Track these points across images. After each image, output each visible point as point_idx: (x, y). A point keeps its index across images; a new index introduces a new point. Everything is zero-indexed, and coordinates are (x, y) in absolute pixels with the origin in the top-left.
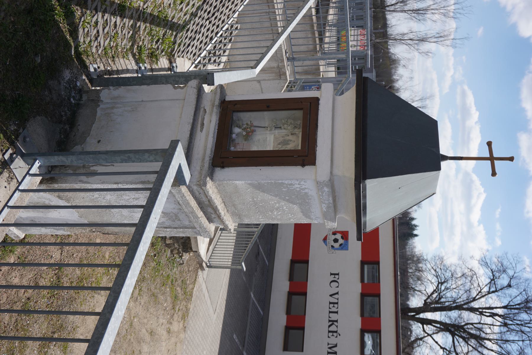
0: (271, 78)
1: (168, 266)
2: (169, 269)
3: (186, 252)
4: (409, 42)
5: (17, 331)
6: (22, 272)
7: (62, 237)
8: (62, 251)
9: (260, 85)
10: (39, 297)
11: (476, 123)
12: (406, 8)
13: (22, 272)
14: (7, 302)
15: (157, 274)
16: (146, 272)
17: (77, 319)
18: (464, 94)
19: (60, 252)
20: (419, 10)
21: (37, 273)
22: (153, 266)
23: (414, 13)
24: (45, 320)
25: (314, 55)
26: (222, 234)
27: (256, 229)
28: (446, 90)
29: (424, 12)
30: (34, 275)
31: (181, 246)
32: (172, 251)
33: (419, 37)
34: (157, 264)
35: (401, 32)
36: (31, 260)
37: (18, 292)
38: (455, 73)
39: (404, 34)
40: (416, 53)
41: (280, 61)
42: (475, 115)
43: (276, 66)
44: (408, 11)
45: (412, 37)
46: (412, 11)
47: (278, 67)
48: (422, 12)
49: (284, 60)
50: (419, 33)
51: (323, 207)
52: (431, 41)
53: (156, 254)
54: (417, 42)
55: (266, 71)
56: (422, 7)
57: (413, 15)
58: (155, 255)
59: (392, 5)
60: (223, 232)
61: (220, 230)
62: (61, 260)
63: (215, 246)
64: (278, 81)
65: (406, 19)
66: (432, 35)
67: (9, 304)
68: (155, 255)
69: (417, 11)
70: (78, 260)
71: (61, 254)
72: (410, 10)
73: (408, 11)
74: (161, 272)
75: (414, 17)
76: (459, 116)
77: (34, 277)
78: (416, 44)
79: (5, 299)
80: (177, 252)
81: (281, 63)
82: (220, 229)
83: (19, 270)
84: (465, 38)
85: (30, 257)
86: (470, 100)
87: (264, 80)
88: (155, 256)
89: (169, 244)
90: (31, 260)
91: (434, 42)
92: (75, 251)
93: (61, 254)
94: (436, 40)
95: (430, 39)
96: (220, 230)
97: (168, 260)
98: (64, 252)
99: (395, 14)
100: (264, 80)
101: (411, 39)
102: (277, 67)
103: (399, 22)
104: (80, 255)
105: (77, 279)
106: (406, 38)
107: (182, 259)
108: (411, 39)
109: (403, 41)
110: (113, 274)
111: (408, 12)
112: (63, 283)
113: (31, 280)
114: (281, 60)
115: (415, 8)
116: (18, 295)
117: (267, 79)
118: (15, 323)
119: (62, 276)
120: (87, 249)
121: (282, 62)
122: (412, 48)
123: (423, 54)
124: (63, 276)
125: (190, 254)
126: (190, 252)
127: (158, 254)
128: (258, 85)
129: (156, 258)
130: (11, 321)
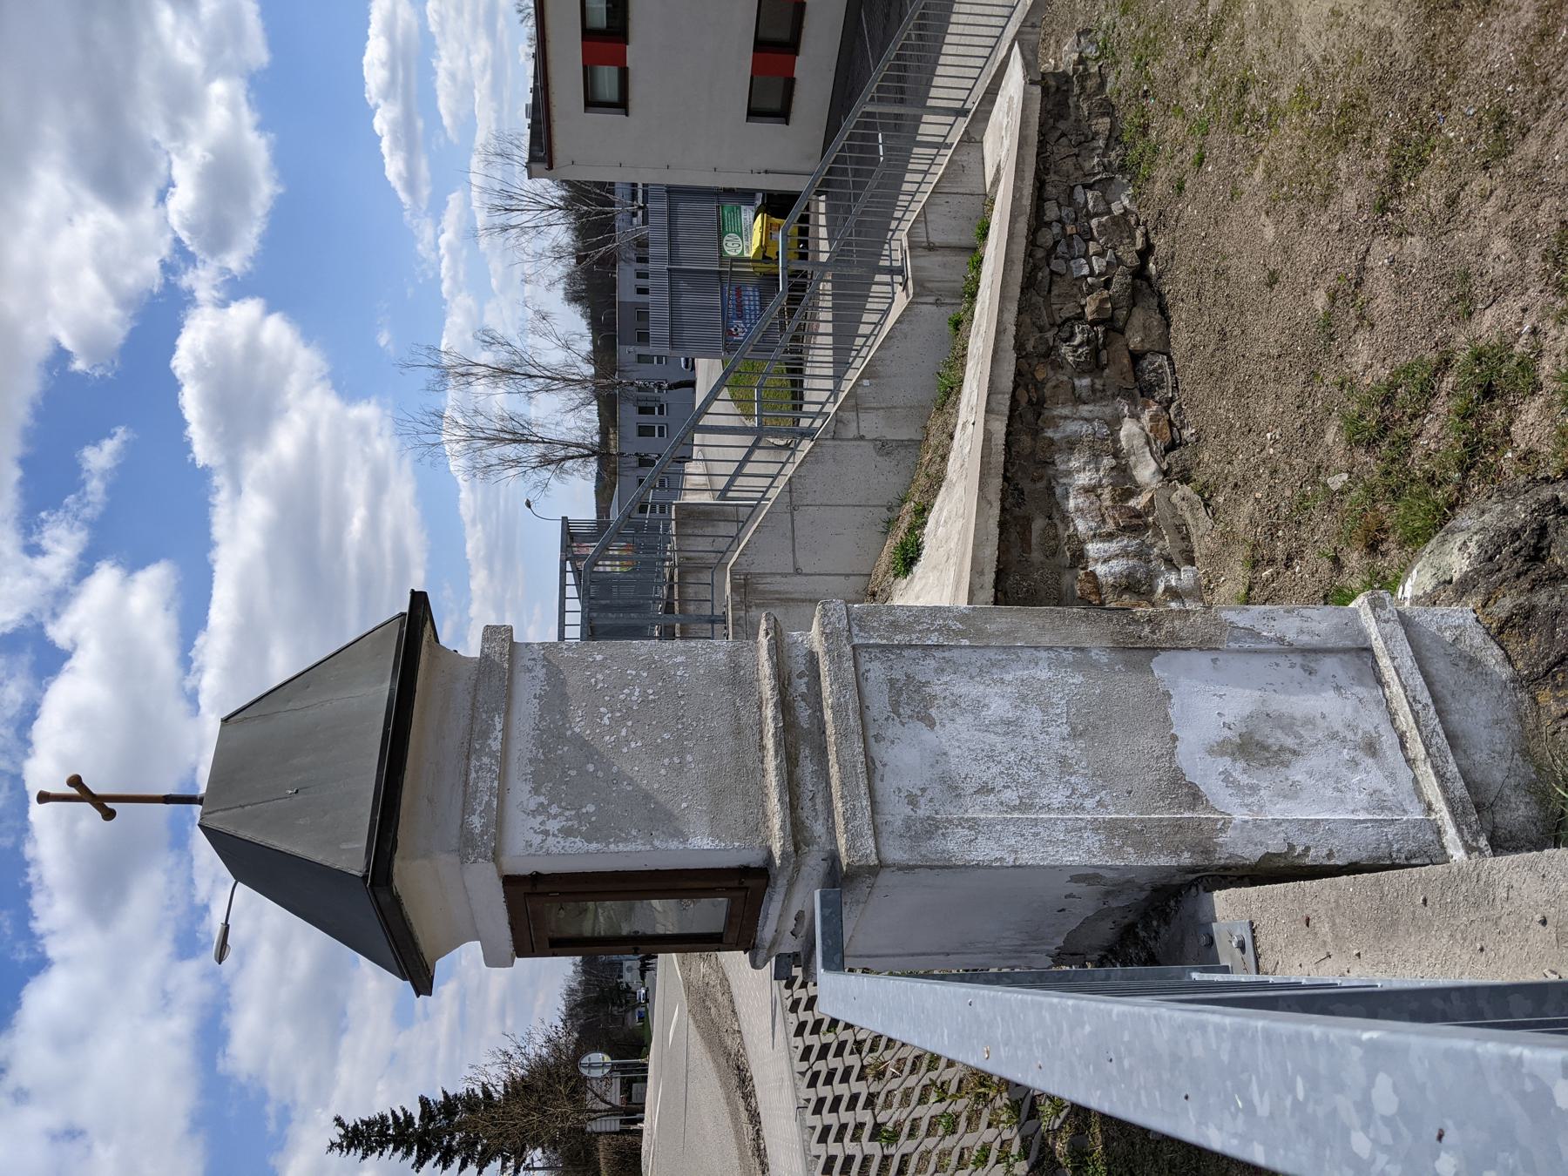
0: (769, 580)
1: (1119, 43)
2: (1119, 35)
3: (1064, 78)
4: (534, 372)
5: (1547, 79)
6: (1476, 262)
7: (1352, 301)
8: (1364, 259)
9: (795, 563)
10: (1459, 153)
11: (377, 106)
12: (541, 448)
13: (1476, 262)
14: (1543, 195)
15: (1152, 35)
16: (1177, 56)
17: (1384, 12)
18: (411, 184)
19: (1368, 258)
20: (515, 441)
21: (1440, 235)
22: (1156, 64)
23: (522, 435)
24: (1467, 63)
25: (685, 561)
26: (963, 94)
27: (869, 109)
28: (454, 200)
29: (502, 435)
30: (1449, 234)
31: (1072, 105)
32: (1102, 85)
33: (511, 381)
34: (1147, 64)
35: (552, 395)
36: (1443, 284)
37: (1507, 206)
38: (437, 237)
39: (548, 390)
40: (518, 344)
41: (742, 622)
42: (381, 124)
43: (754, 608)
44: (537, 442)
45: (527, 382)
46: (527, 441)
47: (748, 608)
48: (507, 436)
49: (733, 625)
50: (512, 390)
51: (500, 736)
52: (483, 369)
53: (1143, 97)
54: (516, 370)
55: (777, 599)
56: (508, 447)
57: (526, 432)
58: (1146, 94)
59: (572, 458)
60: (941, 140)
61: (968, 111)
62: (1373, 232)
63: (990, 55)
64: (754, 569)
65: (542, 426)
66: (482, 381)
67: (1540, 184)
68: (1146, 94)
69: (519, 439)
70: (1331, 206)
71: (1368, 250)
72: (533, 442)
73: (537, 442)
74: (1139, 34)
75: (524, 427)
76: (420, 124)
77: (1451, 225)
78: (518, 366)
79: (1545, 207)
80: (1089, 83)
81: (741, 617)
82: (966, 116)
83: (1481, 275)
84: (408, 366)
85: (1443, 297)
86: (393, 167)
87: (784, 575)
88: (1146, 92)
89: (1103, 115)
90: (1443, 284)
91: (477, 365)
92: (1333, 240)
93: (1368, 250)
94: (475, 370)
95: (486, 373)
96: (952, 144)
97: (1117, 63)
98: (1359, 257)
99: (570, 438)
100: (784, 575)
101: (530, 376)
102: (750, 607)
103: (559, 417)
104: (1324, 220)
105: (1350, 145)
106: (541, 380)
107: (1080, 53)
108: (530, 376)
109: (549, 374)
110: (1261, 98)
111: (536, 439)
112: (1387, 156)
113: (1464, 222)
114: (738, 625)
115: (520, 447)
116: (1510, 196)
117: (778, 578)
118: (1545, 111)
119: (1384, 181)
120: (1302, 227)
121: (738, 620)
122: (526, 357)
123: (502, 341)
124: (1382, 177)
125: (1056, 67)
126: (1053, 74)
127: (1137, 95)
128: (801, 563)
129: (1145, 88)
130: (1553, 124)
